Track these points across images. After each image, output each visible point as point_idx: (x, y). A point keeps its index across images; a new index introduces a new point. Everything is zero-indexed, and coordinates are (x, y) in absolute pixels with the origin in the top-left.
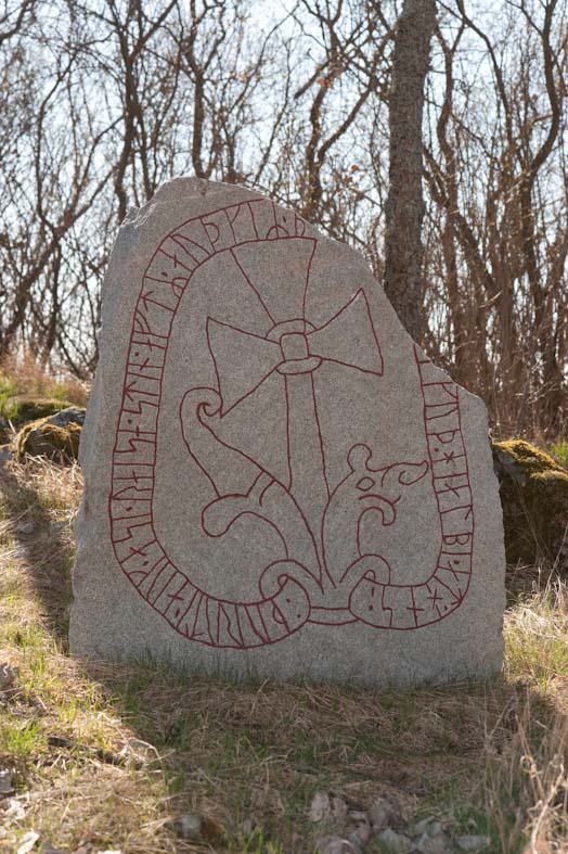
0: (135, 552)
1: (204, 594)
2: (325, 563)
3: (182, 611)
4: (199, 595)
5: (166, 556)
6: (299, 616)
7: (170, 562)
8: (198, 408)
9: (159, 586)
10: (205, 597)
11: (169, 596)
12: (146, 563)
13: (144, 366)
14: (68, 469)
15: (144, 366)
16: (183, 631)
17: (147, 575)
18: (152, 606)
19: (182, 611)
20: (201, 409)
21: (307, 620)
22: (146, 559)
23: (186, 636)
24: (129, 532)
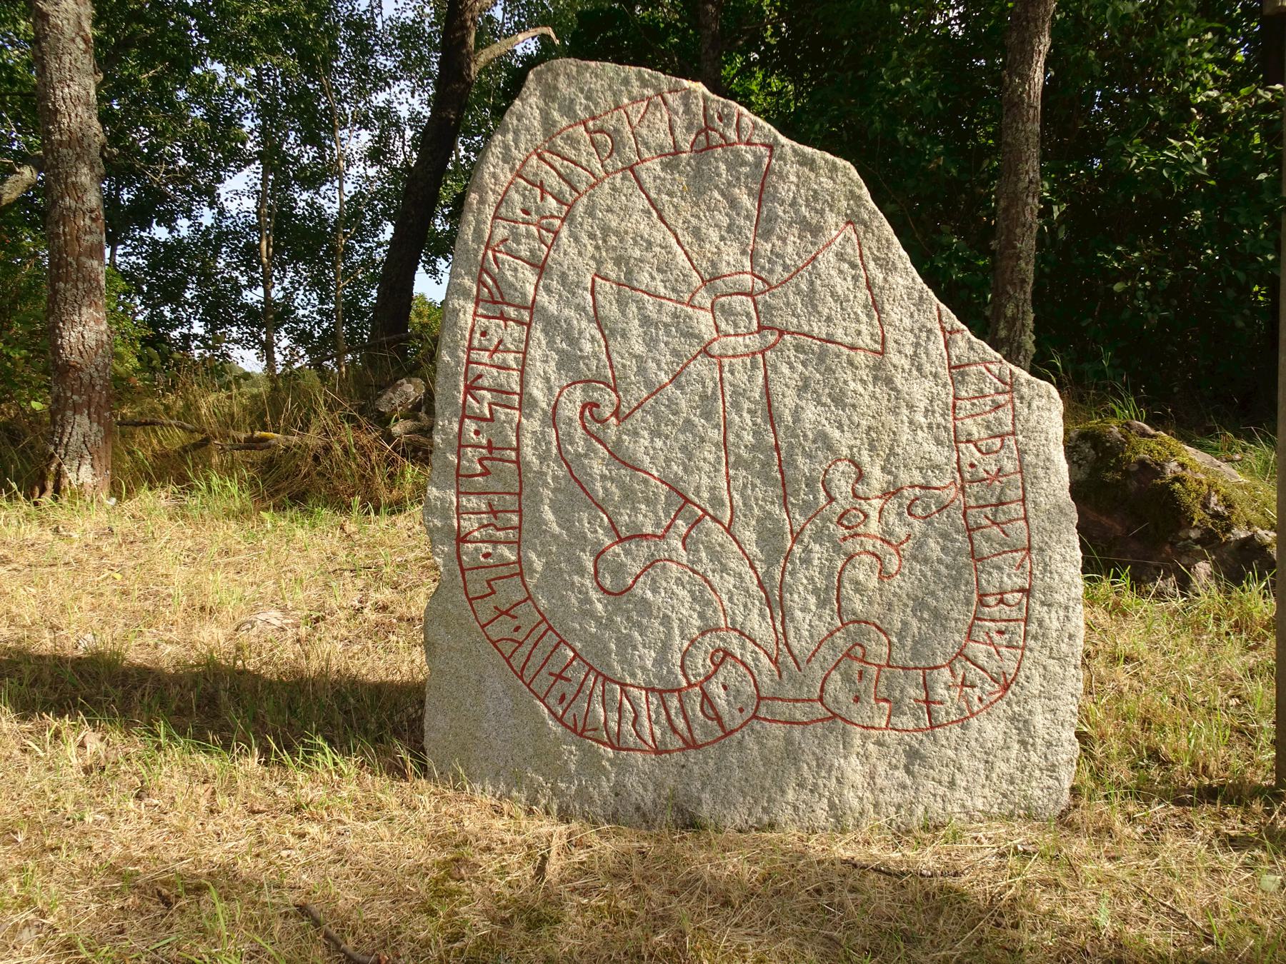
0: (502, 613)
1: (599, 674)
2: (785, 634)
3: (569, 697)
4: (528, 674)
5: (544, 619)
6: (741, 710)
7: (550, 628)
8: (582, 413)
9: (537, 658)
10: (600, 679)
11: (551, 674)
12: (517, 629)
13: (496, 350)
14: (411, 390)
15: (496, 350)
16: (571, 724)
17: (520, 644)
18: (528, 686)
19: (569, 697)
20: (587, 413)
21: (755, 716)
22: (517, 623)
23: (574, 731)
24: (490, 586)
